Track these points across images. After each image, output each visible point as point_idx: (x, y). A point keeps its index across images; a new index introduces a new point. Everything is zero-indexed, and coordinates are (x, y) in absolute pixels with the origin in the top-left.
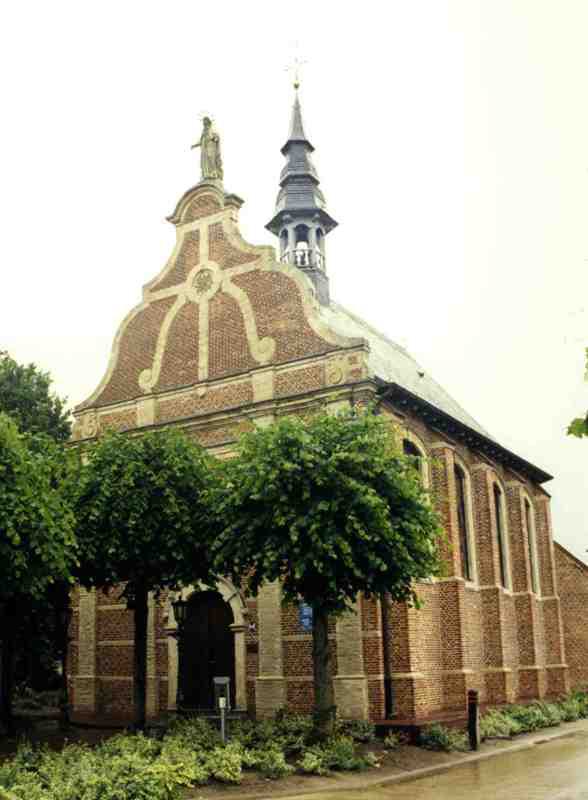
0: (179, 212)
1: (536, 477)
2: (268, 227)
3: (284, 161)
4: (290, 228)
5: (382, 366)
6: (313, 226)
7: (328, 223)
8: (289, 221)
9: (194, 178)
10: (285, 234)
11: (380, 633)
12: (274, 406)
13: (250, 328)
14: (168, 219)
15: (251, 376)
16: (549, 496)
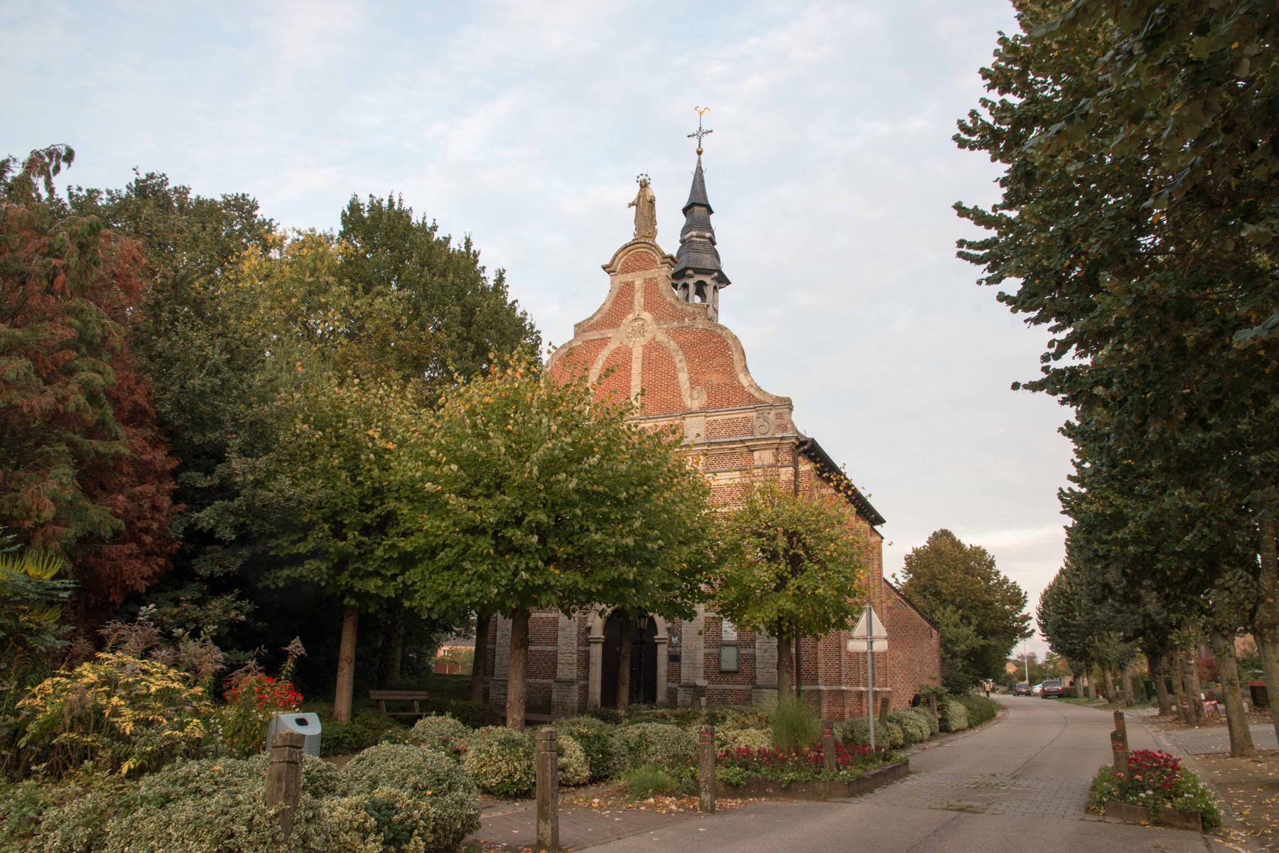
4: (691, 282)
5: (806, 424)
7: (723, 280)
8: (691, 277)
10: (686, 286)
13: (683, 377)
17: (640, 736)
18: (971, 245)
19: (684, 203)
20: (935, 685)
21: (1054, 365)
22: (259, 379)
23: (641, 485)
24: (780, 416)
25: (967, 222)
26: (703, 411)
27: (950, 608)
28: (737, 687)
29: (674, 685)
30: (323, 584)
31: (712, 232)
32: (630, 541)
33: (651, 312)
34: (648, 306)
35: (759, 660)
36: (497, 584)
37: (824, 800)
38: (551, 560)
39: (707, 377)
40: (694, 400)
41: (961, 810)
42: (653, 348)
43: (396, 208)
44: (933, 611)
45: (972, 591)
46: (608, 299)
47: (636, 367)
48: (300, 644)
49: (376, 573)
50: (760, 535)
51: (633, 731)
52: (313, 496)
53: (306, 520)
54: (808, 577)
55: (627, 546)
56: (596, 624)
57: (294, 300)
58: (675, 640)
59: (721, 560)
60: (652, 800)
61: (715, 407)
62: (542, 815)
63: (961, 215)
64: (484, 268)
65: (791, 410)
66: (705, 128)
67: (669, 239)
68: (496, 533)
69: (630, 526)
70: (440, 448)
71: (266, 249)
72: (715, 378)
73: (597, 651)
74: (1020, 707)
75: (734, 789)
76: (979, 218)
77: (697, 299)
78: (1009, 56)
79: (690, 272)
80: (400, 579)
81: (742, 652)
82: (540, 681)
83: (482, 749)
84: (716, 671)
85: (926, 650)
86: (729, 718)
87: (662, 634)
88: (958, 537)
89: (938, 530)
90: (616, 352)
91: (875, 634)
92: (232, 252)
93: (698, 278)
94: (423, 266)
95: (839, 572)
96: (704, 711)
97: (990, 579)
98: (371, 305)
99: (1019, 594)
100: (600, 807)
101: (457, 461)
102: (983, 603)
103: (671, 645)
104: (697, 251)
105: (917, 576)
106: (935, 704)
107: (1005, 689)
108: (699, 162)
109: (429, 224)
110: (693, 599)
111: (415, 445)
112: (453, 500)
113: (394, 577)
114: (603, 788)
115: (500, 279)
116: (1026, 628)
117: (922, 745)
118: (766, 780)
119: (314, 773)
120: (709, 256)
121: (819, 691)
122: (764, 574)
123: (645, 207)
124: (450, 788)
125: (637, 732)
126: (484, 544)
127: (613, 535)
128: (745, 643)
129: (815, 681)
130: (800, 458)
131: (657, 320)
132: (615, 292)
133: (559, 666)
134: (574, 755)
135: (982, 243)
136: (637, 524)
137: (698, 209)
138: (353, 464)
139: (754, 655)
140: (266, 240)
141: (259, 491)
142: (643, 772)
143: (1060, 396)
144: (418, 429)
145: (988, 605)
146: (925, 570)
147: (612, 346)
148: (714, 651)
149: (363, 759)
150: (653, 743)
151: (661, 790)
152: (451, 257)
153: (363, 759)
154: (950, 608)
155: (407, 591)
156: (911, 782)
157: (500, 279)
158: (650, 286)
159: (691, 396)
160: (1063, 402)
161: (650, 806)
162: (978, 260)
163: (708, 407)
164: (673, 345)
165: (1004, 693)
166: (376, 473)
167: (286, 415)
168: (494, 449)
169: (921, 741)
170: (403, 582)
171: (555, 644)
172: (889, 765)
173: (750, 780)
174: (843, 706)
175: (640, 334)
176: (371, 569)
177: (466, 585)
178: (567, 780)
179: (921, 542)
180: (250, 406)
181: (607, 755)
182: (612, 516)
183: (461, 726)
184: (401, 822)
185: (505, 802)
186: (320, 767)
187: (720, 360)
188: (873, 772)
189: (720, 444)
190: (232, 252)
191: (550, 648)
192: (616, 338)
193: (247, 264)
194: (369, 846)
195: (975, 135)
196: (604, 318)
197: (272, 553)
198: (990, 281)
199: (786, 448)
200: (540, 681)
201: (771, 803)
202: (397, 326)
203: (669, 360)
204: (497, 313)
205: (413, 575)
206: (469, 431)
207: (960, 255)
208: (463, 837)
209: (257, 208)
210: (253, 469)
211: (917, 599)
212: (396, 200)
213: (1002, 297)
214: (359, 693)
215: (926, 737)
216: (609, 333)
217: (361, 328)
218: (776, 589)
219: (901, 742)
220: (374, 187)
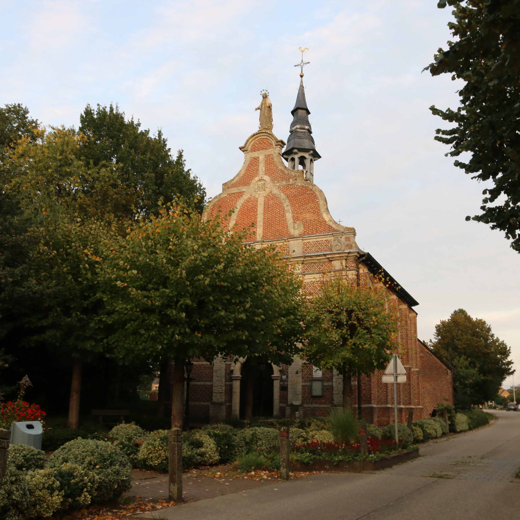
0: (248, 145)
1: (411, 302)
4: (296, 157)
5: (364, 244)
7: (316, 156)
8: (296, 153)
9: (255, 128)
10: (293, 159)
11: (356, 383)
12: (302, 259)
13: (289, 216)
15: (289, 241)
16: (417, 314)
17: (253, 435)
18: (444, 132)
19: (292, 109)
20: (450, 404)
21: (490, 205)
22: (16, 220)
23: (251, 282)
24: (348, 239)
25: (438, 118)
26: (301, 236)
27: (463, 357)
28: (322, 406)
29: (284, 405)
30: (58, 344)
31: (310, 126)
32: (243, 316)
33: (270, 175)
34: (268, 172)
35: (335, 388)
36: (161, 343)
37: (359, 472)
38: (195, 328)
39: (304, 215)
40: (295, 230)
41: (440, 477)
42: (270, 198)
43: (114, 112)
44: (452, 359)
45: (476, 347)
46: (243, 168)
47: (260, 210)
48: (28, 379)
49: (91, 338)
50: (331, 312)
51: (248, 432)
52: (50, 290)
53: (46, 305)
54: (360, 338)
55: (242, 319)
56: (237, 368)
57: (50, 170)
58: (284, 377)
59: (308, 327)
60: (253, 473)
61: (308, 234)
62: (172, 481)
63: (434, 113)
64: (169, 149)
65: (355, 235)
66: (305, 61)
67: (282, 128)
68: (160, 312)
69: (244, 307)
70: (126, 260)
71: (34, 138)
72: (308, 216)
73: (237, 385)
74: (506, 417)
75: (306, 467)
76: (449, 116)
77: (300, 167)
78: (460, 15)
79: (295, 151)
80: (105, 341)
81: (325, 384)
82: (202, 403)
83: (151, 444)
84: (308, 395)
85: (444, 383)
86: (313, 424)
87: (276, 373)
88: (469, 314)
89: (457, 309)
90: (248, 201)
91: (399, 372)
92: (11, 141)
93: (301, 154)
94: (131, 148)
95: (379, 334)
96: (298, 420)
97: (488, 339)
98: (98, 173)
99: (506, 348)
100: (220, 477)
101: (137, 268)
102: (484, 354)
103: (282, 380)
104: (300, 138)
105: (443, 338)
106: (447, 415)
107: (502, 407)
108: (302, 82)
109: (136, 122)
110: (291, 352)
111: (113, 259)
112: (133, 292)
113: (102, 340)
114: (228, 466)
115: (180, 156)
116: (510, 369)
117: (435, 440)
118: (325, 460)
119: (28, 456)
120: (307, 141)
121: (372, 408)
122: (335, 336)
123: (266, 111)
124: (111, 464)
125: (251, 432)
126: (154, 320)
127: (234, 312)
128: (327, 378)
129: (369, 402)
130: (360, 266)
131: (273, 180)
132: (247, 163)
133: (214, 394)
134: (210, 447)
135: (451, 131)
136: (248, 306)
137: (301, 111)
138: (76, 272)
139: (332, 386)
140: (33, 133)
141: (17, 288)
142: (252, 456)
143: (491, 224)
144: (115, 248)
145: (486, 355)
146: (448, 334)
147: (245, 197)
148: (308, 384)
149: (65, 448)
150: (260, 439)
151: (259, 467)
152: (149, 140)
153: (65, 448)
154: (463, 357)
155: (110, 350)
156: (416, 462)
157: (180, 156)
158: (269, 160)
159: (294, 228)
160: (493, 228)
161: (252, 476)
162: (447, 142)
163: (304, 234)
164: (283, 196)
165: (501, 409)
166: (89, 275)
167: (35, 241)
168: (159, 260)
169: (436, 438)
170: (107, 343)
171: (211, 380)
172: (405, 451)
173: (317, 461)
174: (389, 417)
175: (263, 189)
176: (88, 335)
177: (144, 344)
178: (205, 462)
179: (447, 317)
180: (11, 235)
181: (231, 446)
182: (233, 301)
183: (140, 430)
184: (76, 484)
185: (163, 475)
186: (33, 453)
187: (312, 205)
188: (394, 455)
189: (311, 256)
190: (11, 141)
191: (208, 383)
192: (248, 192)
193: (21, 148)
194: (54, 498)
195: (443, 64)
196: (240, 180)
197: (26, 326)
198: (453, 154)
199: (352, 259)
200: (202, 403)
201: (326, 474)
202: (115, 186)
203: (280, 205)
204: (177, 177)
205: (112, 339)
206: (144, 250)
207: (437, 138)
208: (120, 494)
209: (28, 113)
210: (12, 275)
211: (443, 352)
212: (114, 107)
213: (457, 164)
214: (83, 412)
215: (439, 435)
216: (244, 189)
217: (92, 187)
218: (342, 346)
219: (421, 438)
220: (100, 100)
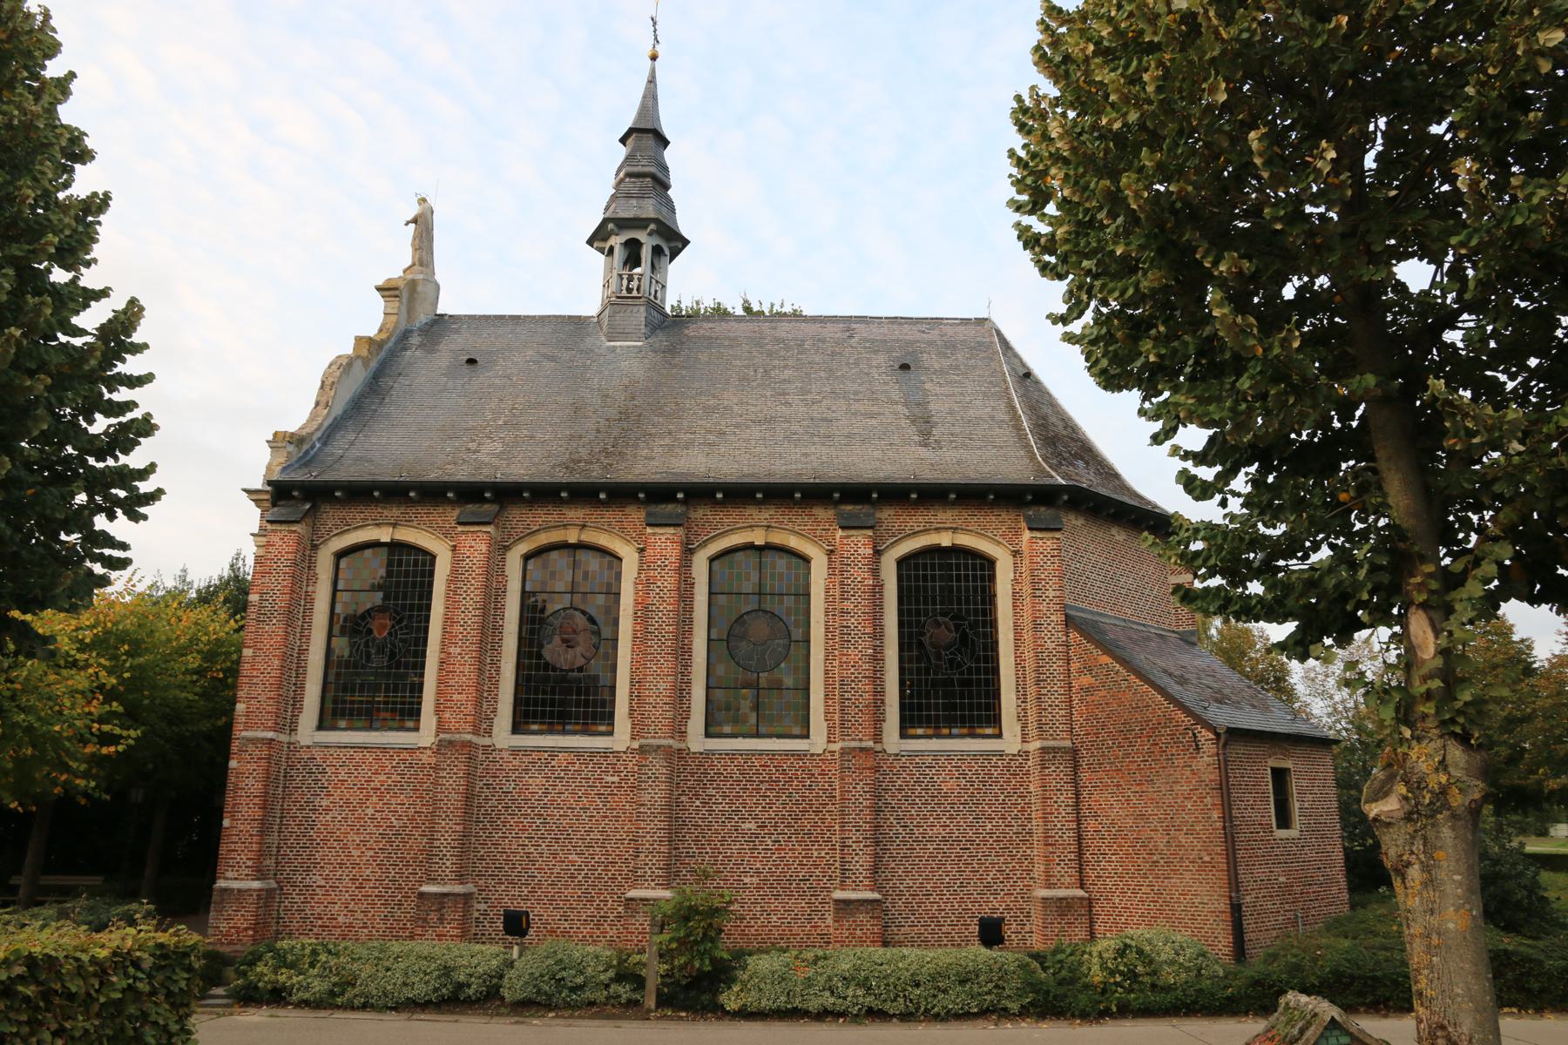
2: (590, 242)
3: (622, 152)
4: (616, 241)
6: (648, 242)
14: (379, 289)
